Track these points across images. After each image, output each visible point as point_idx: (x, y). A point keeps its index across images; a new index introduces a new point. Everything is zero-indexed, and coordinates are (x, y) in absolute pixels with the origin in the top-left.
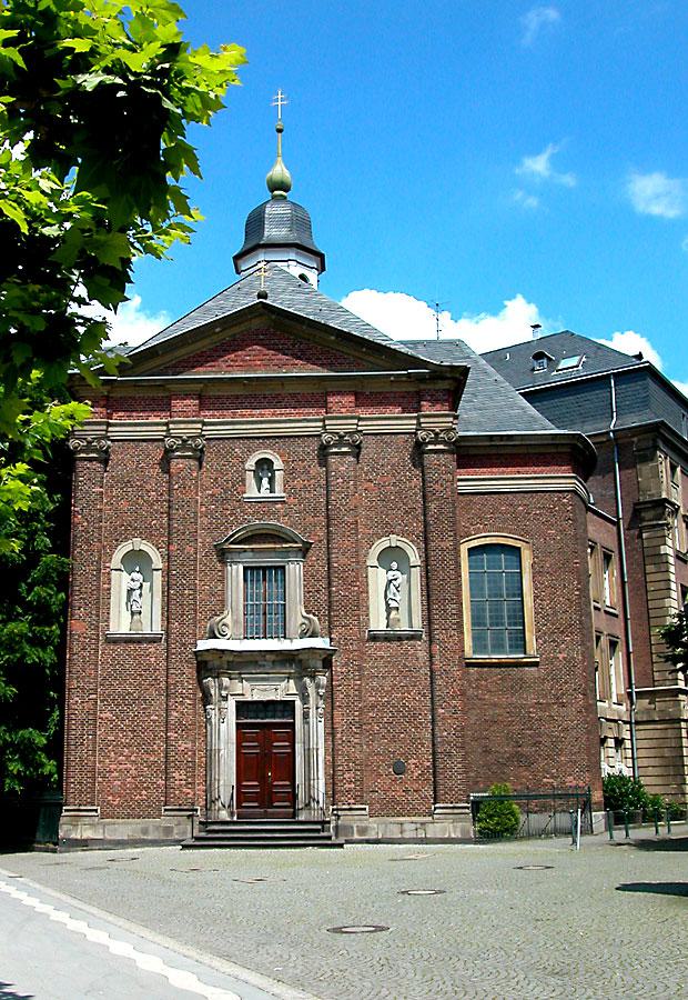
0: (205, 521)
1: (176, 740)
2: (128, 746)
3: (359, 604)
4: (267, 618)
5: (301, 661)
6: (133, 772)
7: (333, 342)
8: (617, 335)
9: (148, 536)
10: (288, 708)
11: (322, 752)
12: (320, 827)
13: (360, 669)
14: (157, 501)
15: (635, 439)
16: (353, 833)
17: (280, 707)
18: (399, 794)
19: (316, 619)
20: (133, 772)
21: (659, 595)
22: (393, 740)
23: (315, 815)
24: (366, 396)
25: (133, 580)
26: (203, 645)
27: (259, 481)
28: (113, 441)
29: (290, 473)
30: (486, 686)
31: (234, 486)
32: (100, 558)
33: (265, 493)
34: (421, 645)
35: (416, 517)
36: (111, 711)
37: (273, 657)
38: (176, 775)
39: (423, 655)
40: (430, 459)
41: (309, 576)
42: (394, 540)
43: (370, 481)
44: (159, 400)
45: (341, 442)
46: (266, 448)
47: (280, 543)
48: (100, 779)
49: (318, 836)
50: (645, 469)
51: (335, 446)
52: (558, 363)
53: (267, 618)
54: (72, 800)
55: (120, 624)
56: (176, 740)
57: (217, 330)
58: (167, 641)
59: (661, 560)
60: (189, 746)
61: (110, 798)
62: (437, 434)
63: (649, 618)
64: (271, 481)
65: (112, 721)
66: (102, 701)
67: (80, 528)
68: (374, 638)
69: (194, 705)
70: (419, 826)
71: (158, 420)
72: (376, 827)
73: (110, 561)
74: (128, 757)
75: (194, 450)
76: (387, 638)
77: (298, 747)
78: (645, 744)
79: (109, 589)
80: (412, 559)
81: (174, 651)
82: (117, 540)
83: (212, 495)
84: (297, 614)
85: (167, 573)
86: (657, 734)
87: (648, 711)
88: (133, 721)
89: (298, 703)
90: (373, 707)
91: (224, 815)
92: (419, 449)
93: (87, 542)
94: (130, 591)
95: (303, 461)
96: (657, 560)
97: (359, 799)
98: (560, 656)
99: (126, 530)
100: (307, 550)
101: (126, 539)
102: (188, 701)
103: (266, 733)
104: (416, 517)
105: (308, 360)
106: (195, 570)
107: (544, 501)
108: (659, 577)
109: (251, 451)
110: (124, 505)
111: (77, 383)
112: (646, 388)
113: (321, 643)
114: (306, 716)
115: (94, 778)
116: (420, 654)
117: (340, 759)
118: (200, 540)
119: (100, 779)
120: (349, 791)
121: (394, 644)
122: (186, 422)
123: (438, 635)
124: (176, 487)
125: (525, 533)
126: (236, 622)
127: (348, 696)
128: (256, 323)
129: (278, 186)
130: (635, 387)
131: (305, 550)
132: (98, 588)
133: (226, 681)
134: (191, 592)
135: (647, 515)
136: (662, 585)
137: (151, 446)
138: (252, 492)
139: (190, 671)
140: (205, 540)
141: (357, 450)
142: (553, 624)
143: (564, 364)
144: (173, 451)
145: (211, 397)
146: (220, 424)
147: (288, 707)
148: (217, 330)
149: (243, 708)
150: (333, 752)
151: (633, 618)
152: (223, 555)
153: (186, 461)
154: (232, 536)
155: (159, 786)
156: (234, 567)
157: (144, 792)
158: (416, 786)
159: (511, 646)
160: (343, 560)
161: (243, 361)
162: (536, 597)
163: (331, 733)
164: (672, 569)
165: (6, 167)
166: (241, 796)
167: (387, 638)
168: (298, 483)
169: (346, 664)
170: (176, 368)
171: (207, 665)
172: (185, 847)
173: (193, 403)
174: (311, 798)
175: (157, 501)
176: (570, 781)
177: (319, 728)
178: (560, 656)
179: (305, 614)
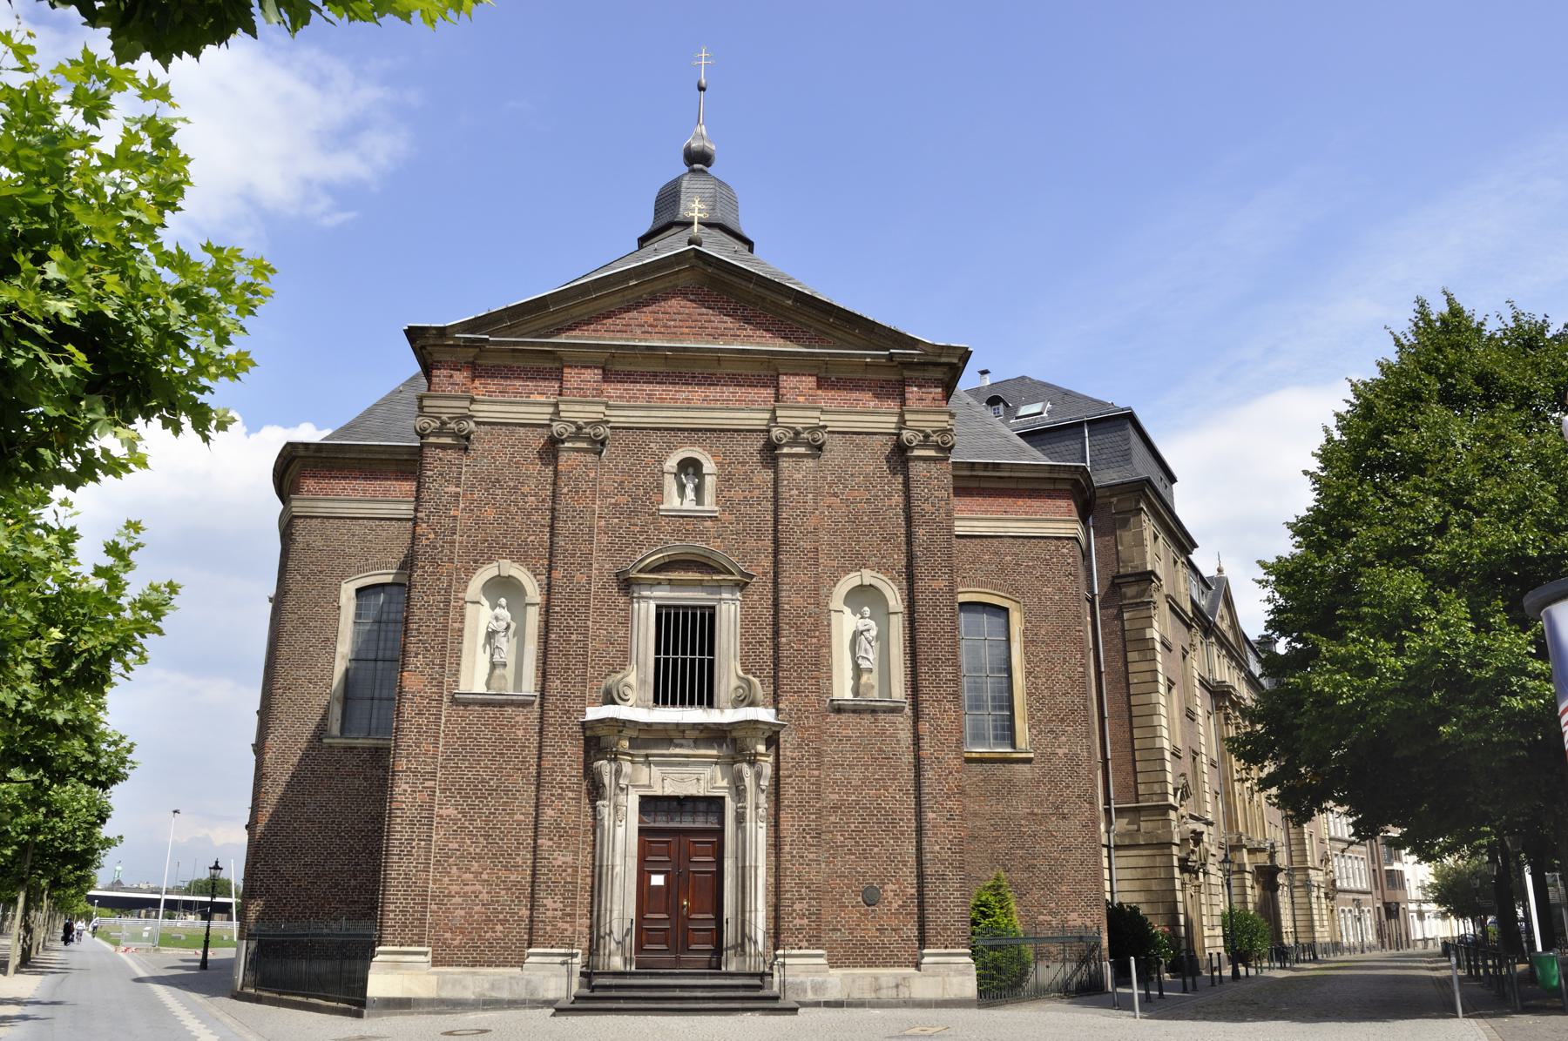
0: (605, 539)
1: (551, 850)
2: (480, 857)
3: (819, 663)
5: (734, 740)
6: (485, 896)
7: (788, 308)
9: (521, 557)
10: (714, 808)
11: (762, 872)
12: (757, 982)
13: (819, 754)
14: (537, 509)
15: (1114, 500)
17: (702, 806)
18: (870, 931)
19: (756, 681)
20: (485, 896)
21: (1144, 688)
22: (864, 855)
23: (751, 965)
24: (829, 377)
25: (497, 619)
26: (594, 713)
27: (682, 488)
28: (477, 423)
29: (725, 480)
31: (646, 493)
32: (450, 586)
33: (689, 503)
34: (903, 724)
35: (898, 546)
36: (456, 806)
37: (695, 734)
38: (548, 902)
39: (905, 736)
40: (917, 469)
42: (868, 577)
43: (835, 495)
44: (549, 367)
45: (796, 439)
46: (693, 445)
48: (434, 907)
49: (756, 995)
50: (1126, 536)
51: (788, 444)
52: (1016, 409)
54: (390, 938)
55: (474, 678)
56: (551, 850)
58: (542, 705)
59: (1145, 646)
60: (569, 859)
61: (448, 935)
62: (927, 436)
63: (1131, 717)
64: (699, 490)
65: (455, 821)
66: (443, 791)
67: (425, 542)
68: (839, 710)
69: (578, 800)
71: (543, 399)
72: (837, 981)
73: (464, 590)
74: (477, 874)
75: (592, 441)
77: (729, 865)
78: (1127, 874)
79: (461, 630)
80: (892, 603)
81: (552, 721)
82: (476, 561)
85: (547, 610)
86: (1142, 862)
87: (1130, 834)
89: (730, 807)
90: (835, 808)
91: (617, 963)
92: (900, 455)
93: (433, 561)
94: (491, 635)
95: (743, 464)
96: (1141, 646)
97: (815, 941)
98: (1060, 752)
99: (490, 547)
101: (490, 560)
102: (571, 795)
103: (684, 839)
104: (898, 546)
105: (759, 326)
106: (587, 606)
107: (1039, 549)
108: (1145, 666)
109: (671, 448)
110: (490, 513)
111: (431, 342)
112: (1127, 440)
113: (765, 714)
114: (740, 818)
115: (424, 905)
117: (788, 883)
118: (595, 566)
119: (434, 907)
121: (868, 718)
122: (585, 403)
123: (928, 708)
124: (565, 490)
125: (1015, 591)
126: (643, 682)
127: (801, 791)
129: (698, 159)
130: (1111, 439)
131: (741, 586)
132: (446, 627)
133: (627, 767)
134: (581, 637)
135: (1130, 591)
136: (1148, 677)
137: (530, 432)
138: (673, 501)
140: (602, 568)
141: (817, 449)
142: (1050, 709)
143: (1024, 411)
144: (563, 442)
145: (619, 366)
146: (631, 407)
147: (714, 805)
149: (649, 804)
150: (777, 872)
151: (1111, 717)
152: (627, 585)
153: (580, 457)
155: (521, 919)
156: (643, 605)
157: (499, 928)
159: (996, 737)
160: (797, 600)
162: (1029, 673)
163: (776, 845)
164: (1159, 658)
166: (643, 932)
167: (856, 710)
168: (736, 494)
169: (800, 746)
171: (597, 742)
172: (560, 1011)
173: (592, 375)
174: (744, 938)
175: (537, 509)
176: (1075, 920)
177: (759, 834)
178: (1060, 752)
179: (741, 673)
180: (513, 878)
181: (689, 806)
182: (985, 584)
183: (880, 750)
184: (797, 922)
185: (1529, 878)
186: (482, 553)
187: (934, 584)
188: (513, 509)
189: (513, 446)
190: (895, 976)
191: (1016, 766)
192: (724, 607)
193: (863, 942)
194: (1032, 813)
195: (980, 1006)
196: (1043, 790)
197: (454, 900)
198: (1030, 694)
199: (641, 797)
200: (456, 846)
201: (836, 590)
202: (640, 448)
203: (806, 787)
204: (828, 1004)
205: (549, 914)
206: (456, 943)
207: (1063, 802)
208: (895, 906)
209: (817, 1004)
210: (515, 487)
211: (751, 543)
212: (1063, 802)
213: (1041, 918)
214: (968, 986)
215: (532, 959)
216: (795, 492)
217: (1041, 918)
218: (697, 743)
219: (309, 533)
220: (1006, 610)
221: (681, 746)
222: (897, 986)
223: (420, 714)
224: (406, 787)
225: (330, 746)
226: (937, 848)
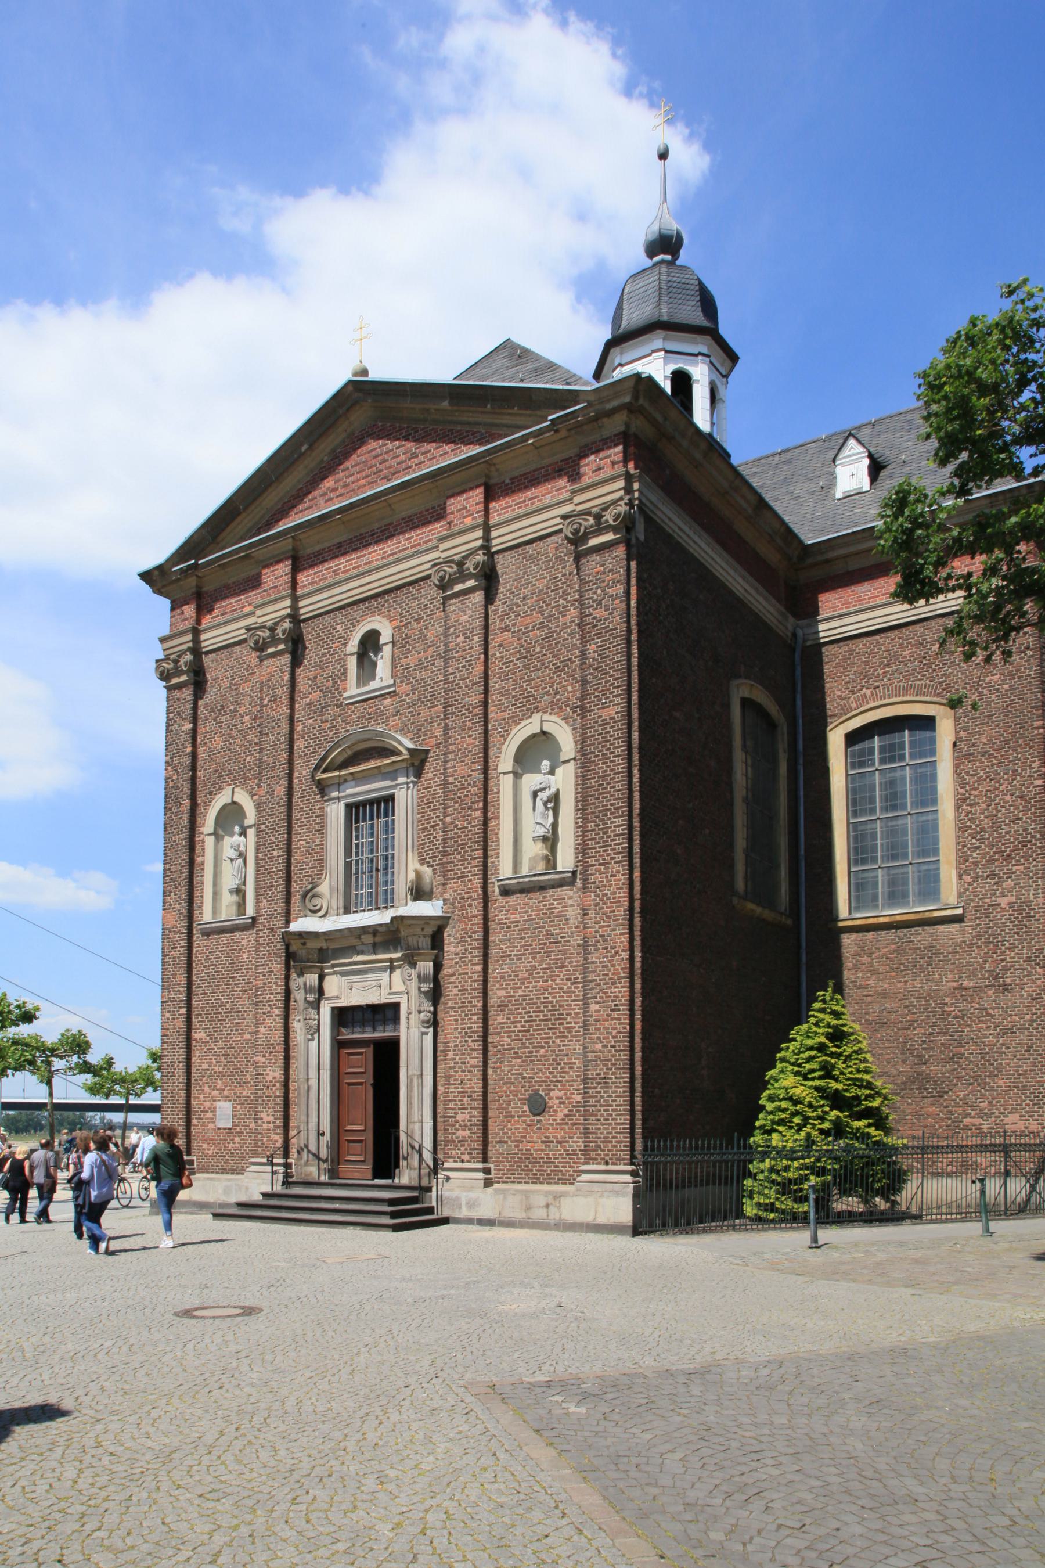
4: (367, 876)
8: (540, 26)
16: (460, 1208)
18: (535, 1145)
22: (530, 1058)
30: (871, 964)
38: (263, 1115)
41: (424, 803)
47: (387, 757)
53: (367, 876)
57: (304, 448)
62: (598, 517)
72: (488, 1202)
76: (525, 889)
83: (310, 704)
84: (409, 867)
98: (1003, 902)
100: (423, 762)
128: (359, 417)
138: (352, 690)
142: (991, 845)
148: (304, 448)
149: (343, 1016)
154: (323, 759)
157: (237, 1139)
158: (560, 1134)
168: (412, 660)
169: (462, 940)
170: (269, 525)
178: (1003, 902)
181: (359, 1015)
182: (905, 690)
183: (549, 934)
188: (234, 733)
190: (547, 1193)
191: (941, 928)
192: (403, 792)
193: (528, 1156)
194: (961, 988)
195: (637, 1231)
196: (977, 956)
199: (333, 1009)
204: (481, 1222)
206: (210, 1153)
208: (560, 1115)
209: (469, 1221)
210: (235, 710)
211: (426, 712)
212: (1005, 969)
213: (967, 1121)
214: (621, 1208)
215: (253, 1168)
217: (967, 1121)
218: (375, 948)
221: (362, 953)
222: (547, 1206)
226: (599, 1046)
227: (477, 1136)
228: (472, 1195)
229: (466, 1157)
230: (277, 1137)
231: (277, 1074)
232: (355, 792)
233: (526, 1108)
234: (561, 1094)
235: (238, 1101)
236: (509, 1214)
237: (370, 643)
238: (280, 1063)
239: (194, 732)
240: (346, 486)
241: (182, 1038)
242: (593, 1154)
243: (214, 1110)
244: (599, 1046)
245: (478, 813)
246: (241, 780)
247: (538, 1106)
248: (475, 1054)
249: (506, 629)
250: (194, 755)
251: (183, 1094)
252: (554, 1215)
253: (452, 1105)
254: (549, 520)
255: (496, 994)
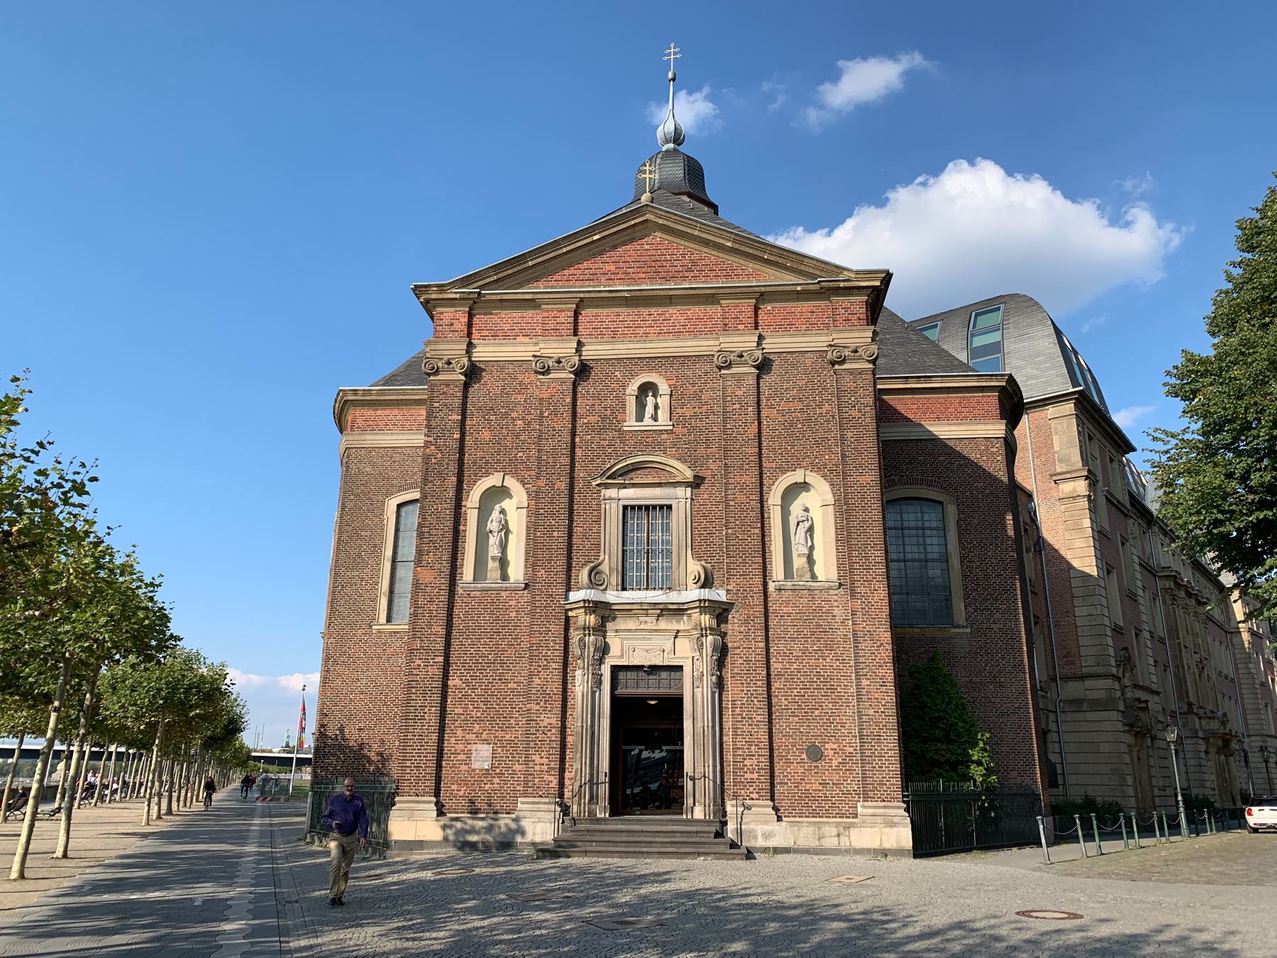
2: (480, 720)
38: (536, 758)
46: (651, 371)
70: (842, 830)
72: (781, 834)
74: (478, 734)
88: (486, 690)
98: (995, 627)
109: (633, 375)
116: (836, 612)
120: (752, 782)
138: (631, 424)
139: (23, 882)
142: (985, 589)
154: (609, 469)
157: (496, 780)
161: (625, 273)
165: (4, 446)
169: (746, 622)
178: (995, 627)
180: (507, 737)
183: (818, 625)
184: (748, 776)
185: (317, 893)
186: (480, 468)
187: (862, 479)
189: (504, 380)
190: (838, 824)
194: (971, 682)
197: (460, 757)
198: (965, 576)
200: (461, 711)
201: (774, 488)
202: (607, 376)
203: (752, 657)
204: (777, 851)
205: (537, 768)
206: (461, 793)
207: (999, 672)
208: (835, 763)
214: (903, 835)
216: (737, 406)
219: (360, 462)
220: (941, 503)
222: (838, 835)
223: (431, 601)
224: (418, 662)
225: (379, 632)
227: (765, 778)
228: (767, 828)
229: (755, 796)
230: (552, 778)
231: (555, 720)
232: (630, 495)
233: (804, 756)
234: (835, 746)
235: (498, 743)
236: (802, 843)
237: (647, 389)
238: (558, 711)
239: (463, 421)
240: (625, 273)
241: (438, 684)
242: (871, 794)
243: (469, 753)
244: (871, 712)
245: (757, 531)
246: (512, 468)
247: (815, 754)
248: (761, 712)
249: (772, 407)
250: (462, 441)
251: (435, 737)
252: (845, 842)
253: (740, 752)
254: (818, 341)
255: (776, 666)
